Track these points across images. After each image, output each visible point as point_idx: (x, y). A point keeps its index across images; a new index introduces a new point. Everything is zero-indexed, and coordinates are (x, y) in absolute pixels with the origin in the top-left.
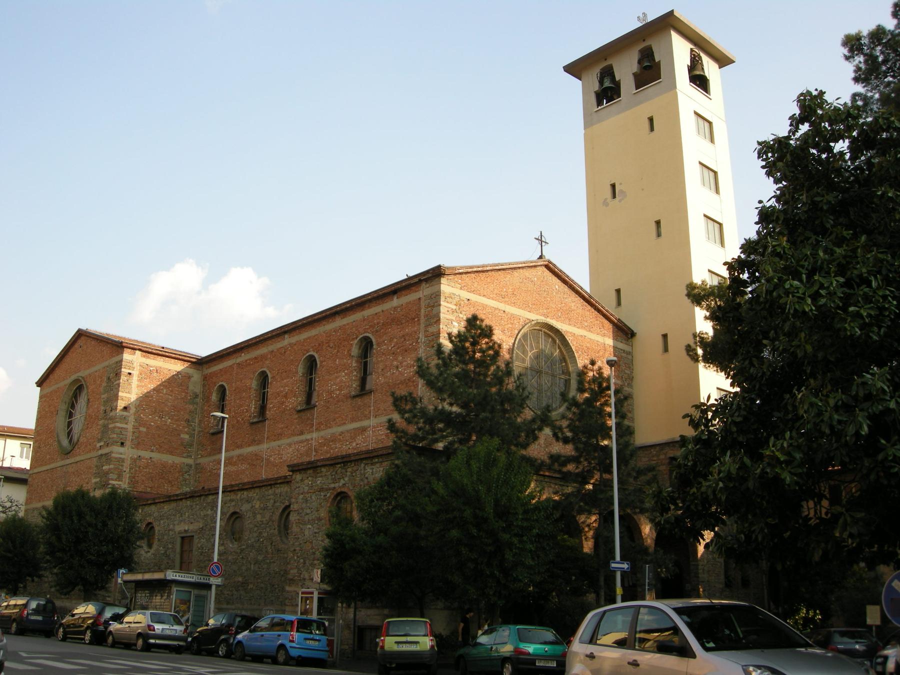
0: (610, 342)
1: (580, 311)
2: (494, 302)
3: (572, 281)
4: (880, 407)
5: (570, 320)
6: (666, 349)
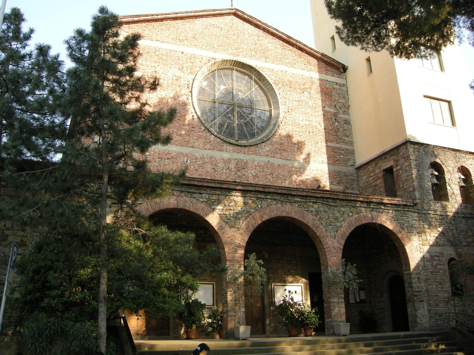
1: (280, 50)
3: (266, 24)
4: (31, 121)
5: (266, 58)
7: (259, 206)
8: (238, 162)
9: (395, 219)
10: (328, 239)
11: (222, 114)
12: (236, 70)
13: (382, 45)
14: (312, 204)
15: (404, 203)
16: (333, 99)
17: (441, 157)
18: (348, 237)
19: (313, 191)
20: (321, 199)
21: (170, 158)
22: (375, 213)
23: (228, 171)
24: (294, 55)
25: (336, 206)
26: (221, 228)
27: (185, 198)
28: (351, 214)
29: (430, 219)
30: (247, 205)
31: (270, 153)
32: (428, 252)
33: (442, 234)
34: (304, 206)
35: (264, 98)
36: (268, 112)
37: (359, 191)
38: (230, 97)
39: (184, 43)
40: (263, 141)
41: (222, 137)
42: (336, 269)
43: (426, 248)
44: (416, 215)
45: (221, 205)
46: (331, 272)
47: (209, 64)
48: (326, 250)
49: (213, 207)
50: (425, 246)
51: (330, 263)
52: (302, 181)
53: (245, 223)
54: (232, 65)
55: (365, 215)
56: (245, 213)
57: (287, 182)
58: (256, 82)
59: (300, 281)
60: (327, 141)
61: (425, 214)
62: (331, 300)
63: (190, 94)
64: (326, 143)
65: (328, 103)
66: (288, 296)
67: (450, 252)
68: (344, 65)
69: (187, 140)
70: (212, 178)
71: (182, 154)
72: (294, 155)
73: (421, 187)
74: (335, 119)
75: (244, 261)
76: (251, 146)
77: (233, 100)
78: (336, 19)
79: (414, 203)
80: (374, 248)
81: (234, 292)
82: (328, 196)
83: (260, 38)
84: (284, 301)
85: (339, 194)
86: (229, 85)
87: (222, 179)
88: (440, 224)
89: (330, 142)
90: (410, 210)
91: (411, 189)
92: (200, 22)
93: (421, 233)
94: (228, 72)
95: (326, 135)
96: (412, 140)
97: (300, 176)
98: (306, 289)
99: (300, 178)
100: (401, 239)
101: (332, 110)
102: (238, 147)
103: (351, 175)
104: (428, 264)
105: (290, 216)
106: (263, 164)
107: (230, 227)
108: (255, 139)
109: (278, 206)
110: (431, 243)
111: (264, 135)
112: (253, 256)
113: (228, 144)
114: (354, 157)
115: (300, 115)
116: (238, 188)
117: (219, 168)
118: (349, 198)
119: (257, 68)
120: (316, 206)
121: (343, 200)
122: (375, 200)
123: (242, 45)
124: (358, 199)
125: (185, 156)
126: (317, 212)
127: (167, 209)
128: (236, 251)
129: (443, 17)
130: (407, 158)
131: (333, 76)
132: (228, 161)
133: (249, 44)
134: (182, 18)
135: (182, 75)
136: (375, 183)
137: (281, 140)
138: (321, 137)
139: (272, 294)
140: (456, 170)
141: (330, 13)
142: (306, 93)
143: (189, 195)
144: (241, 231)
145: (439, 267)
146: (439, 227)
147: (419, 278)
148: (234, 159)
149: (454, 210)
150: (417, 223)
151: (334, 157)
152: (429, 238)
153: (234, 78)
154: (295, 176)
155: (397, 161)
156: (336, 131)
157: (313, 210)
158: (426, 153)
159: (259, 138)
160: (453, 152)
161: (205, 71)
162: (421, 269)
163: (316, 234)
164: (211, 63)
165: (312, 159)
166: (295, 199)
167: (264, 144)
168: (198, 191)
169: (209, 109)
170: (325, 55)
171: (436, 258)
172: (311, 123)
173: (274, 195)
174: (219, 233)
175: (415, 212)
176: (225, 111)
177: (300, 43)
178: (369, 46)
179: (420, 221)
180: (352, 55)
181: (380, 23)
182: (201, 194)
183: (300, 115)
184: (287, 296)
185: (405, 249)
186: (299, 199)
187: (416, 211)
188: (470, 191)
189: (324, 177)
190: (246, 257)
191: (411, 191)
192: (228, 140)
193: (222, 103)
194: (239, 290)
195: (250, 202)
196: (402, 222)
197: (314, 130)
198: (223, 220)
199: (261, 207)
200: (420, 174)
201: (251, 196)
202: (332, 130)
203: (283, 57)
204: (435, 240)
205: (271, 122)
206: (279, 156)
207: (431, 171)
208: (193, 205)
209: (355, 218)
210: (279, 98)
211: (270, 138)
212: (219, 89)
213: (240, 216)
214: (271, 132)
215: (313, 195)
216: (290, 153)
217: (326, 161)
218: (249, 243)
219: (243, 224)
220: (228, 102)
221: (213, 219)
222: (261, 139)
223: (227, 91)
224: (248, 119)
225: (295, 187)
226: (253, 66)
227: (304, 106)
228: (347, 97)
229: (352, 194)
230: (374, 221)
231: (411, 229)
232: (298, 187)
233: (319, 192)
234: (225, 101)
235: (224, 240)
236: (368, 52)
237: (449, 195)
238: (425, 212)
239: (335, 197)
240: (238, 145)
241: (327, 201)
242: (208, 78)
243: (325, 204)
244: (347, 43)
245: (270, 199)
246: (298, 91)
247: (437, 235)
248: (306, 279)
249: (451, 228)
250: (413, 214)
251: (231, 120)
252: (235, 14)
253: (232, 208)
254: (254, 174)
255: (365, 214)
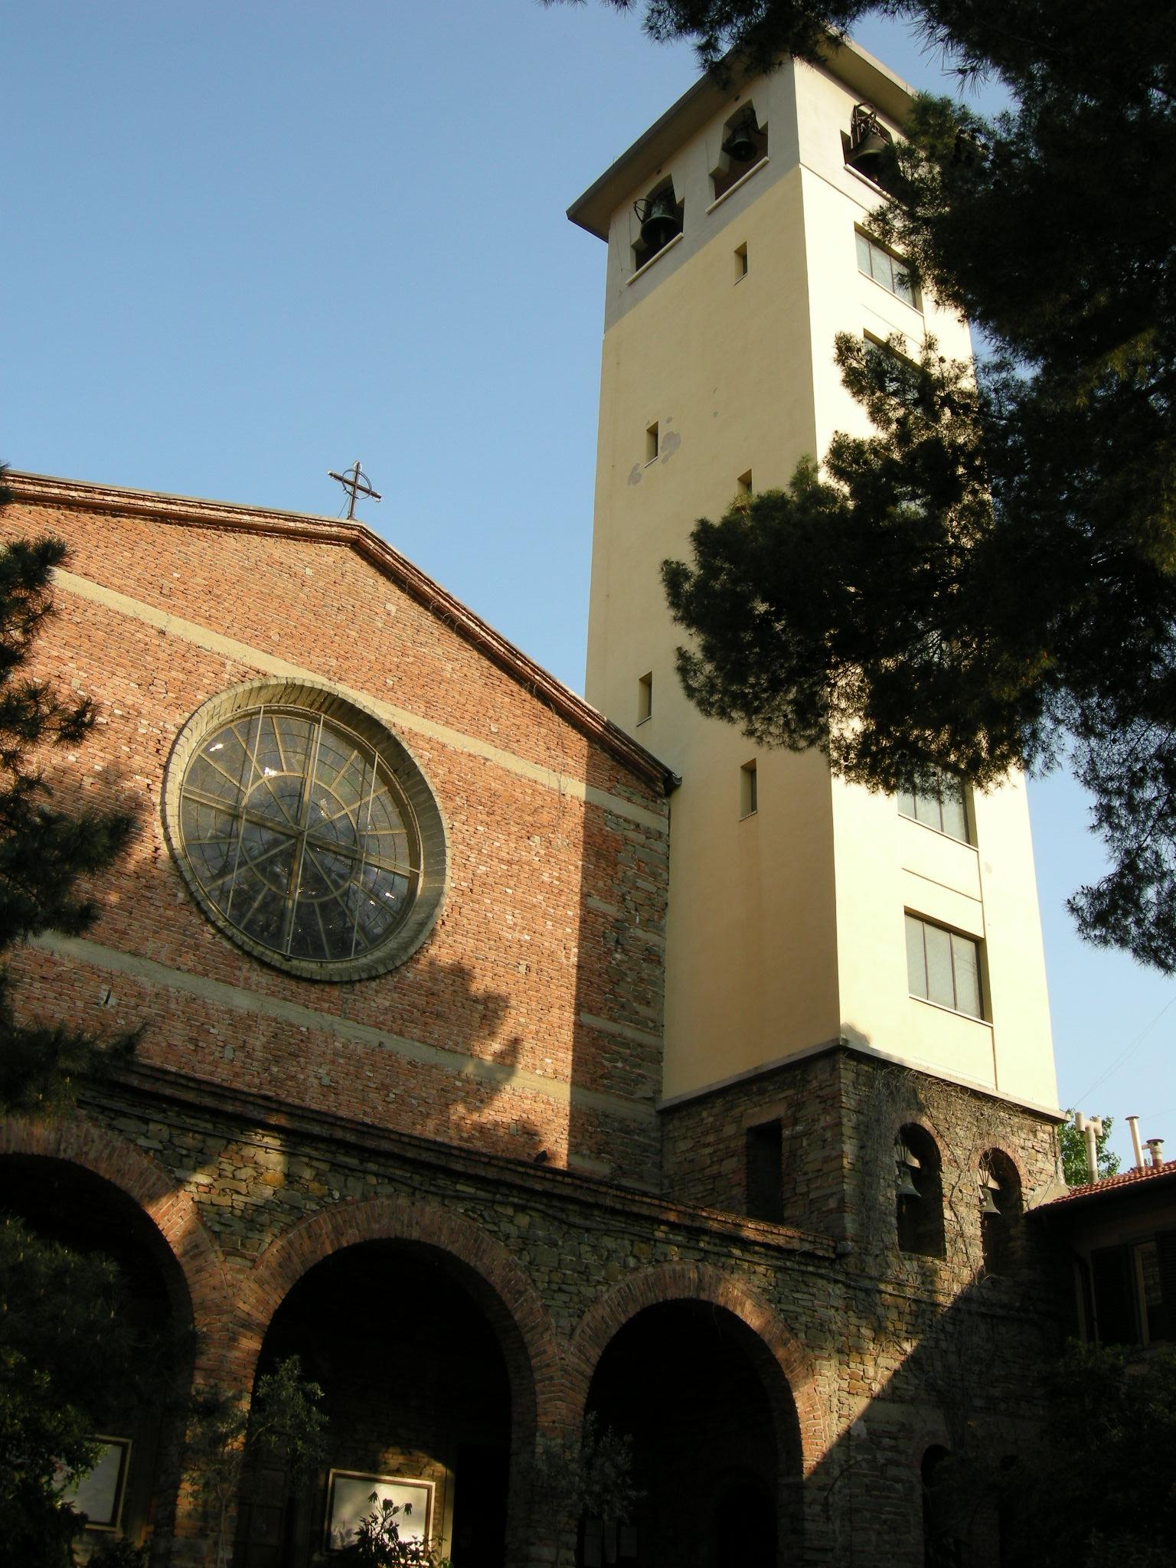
0: (576, 789)
1: (477, 688)
2: (125, 599)
3: (447, 597)
5: (429, 704)
6: (752, 804)
7: (337, 1195)
8: (280, 1030)
9: (771, 1298)
10: (547, 1337)
11: (253, 858)
12: (326, 725)
13: (812, 732)
14: (510, 1211)
15: (807, 1247)
16: (620, 875)
17: (935, 1113)
18: (614, 1338)
19: (521, 1169)
20: (545, 1201)
21: (52, 976)
22: (710, 1269)
23: (241, 1055)
24: (518, 712)
25: (588, 1230)
26: (195, 1249)
27: (87, 1125)
28: (632, 1262)
29: (880, 1310)
30: (296, 1186)
31: (389, 1017)
32: (866, 1417)
33: (912, 1363)
34: (486, 1214)
35: (402, 831)
36: (405, 882)
37: (660, 1185)
38: (287, 812)
39: (174, 601)
40: (374, 973)
41: (241, 938)
42: (563, 1446)
43: (860, 1404)
44: (839, 1290)
45: (208, 1169)
46: (547, 1451)
47: (240, 689)
48: (537, 1376)
49: (179, 1173)
50: (857, 1399)
51: (544, 1421)
52: (481, 1129)
53: (279, 1243)
54: (317, 705)
55: (680, 1271)
56: (286, 1210)
57: (431, 1125)
58: (381, 773)
59: (428, 1471)
60: (579, 1009)
61: (867, 1291)
62: (534, 1551)
63: (160, 772)
64: (577, 1013)
65: (601, 884)
66: (380, 1520)
67: (932, 1424)
68: (670, 773)
69: (121, 926)
70: (183, 1072)
71: (94, 970)
72: (467, 1038)
73: (866, 1202)
74: (617, 942)
75: (257, 1379)
76: (331, 983)
77: (297, 822)
78: (689, 626)
79: (839, 1250)
80: (697, 1387)
81: (206, 1485)
82: (567, 1191)
83: (422, 638)
84: (364, 1533)
85: (603, 1189)
86: (293, 770)
87: (217, 1081)
88: (910, 1328)
89: (590, 1012)
90: (823, 1271)
91: (832, 1204)
92: (239, 546)
93: (848, 1351)
94: (298, 725)
95: (578, 988)
96: (854, 1045)
97: (479, 1110)
98: (441, 1500)
99: (475, 1117)
100: (783, 1366)
101: (612, 910)
102: (287, 981)
103: (643, 1131)
104: (859, 1458)
105: (433, 1240)
106: (360, 1050)
107: (227, 1254)
108: (348, 965)
109: (399, 1202)
110: (876, 1388)
111: (378, 954)
112: (290, 1367)
113: (255, 966)
114: (659, 1071)
115: (508, 909)
116: (273, 1120)
117: (211, 1039)
118: (635, 1209)
119: (394, 732)
120: (523, 1220)
121: (613, 1211)
122: (715, 1226)
123: (360, 649)
124: (664, 1217)
125: (105, 980)
126: (526, 1241)
127: (17, 1155)
128: (234, 1339)
129: (1026, 682)
130: (832, 1101)
131: (629, 800)
132: (244, 1023)
133: (384, 649)
134: (183, 520)
135: (146, 705)
136: (715, 1169)
137: (434, 980)
138: (564, 991)
139: (324, 1506)
140: (976, 1159)
141: (674, 605)
142: (537, 839)
143: (103, 1120)
144: (262, 1271)
145: (892, 1471)
146: (907, 1339)
147: (826, 1505)
148: (268, 1019)
149: (956, 1288)
150: (838, 1318)
151: (596, 1062)
152: (871, 1372)
153: (316, 750)
154: (461, 1109)
155: (797, 1106)
156: (616, 978)
157: (513, 1231)
158: (891, 1093)
159: (363, 961)
160: (974, 1102)
161: (224, 706)
162: (836, 1472)
163: (509, 1315)
164: (248, 686)
165: (524, 1060)
166: (459, 1187)
167: (374, 984)
168: (137, 1111)
169: (211, 838)
170: (618, 731)
171: (886, 1441)
172: (538, 938)
173: (391, 1163)
174: (185, 1268)
175: (836, 1281)
176: (266, 851)
177: (545, 676)
178: (772, 729)
179: (851, 1313)
180: (705, 748)
181: (813, 669)
182: (147, 1121)
183: (508, 909)
184: (376, 1519)
185: (792, 1402)
186: (472, 1190)
187: (840, 1277)
188: (1012, 1232)
189: (553, 1126)
190: (265, 1363)
191: (831, 1211)
192: (258, 950)
193: (259, 824)
194: (224, 1480)
195: (308, 1174)
196: (792, 1308)
197: (545, 965)
198: (204, 1224)
199: (343, 1198)
200: (867, 1158)
201: (314, 1153)
202: (600, 975)
203: (482, 711)
204: (890, 1381)
205: (412, 916)
206: (417, 1032)
207: (899, 1153)
208: (110, 1156)
209: (646, 1276)
210: (448, 843)
211: (397, 968)
212: (258, 777)
213: (265, 1218)
214: (404, 947)
215: (518, 1181)
216: (455, 1030)
217: (568, 1071)
218: (282, 1315)
219: (271, 1247)
220: (279, 823)
221: (172, 1216)
222: (369, 968)
223: (281, 790)
224: (336, 894)
225: (455, 1143)
226: (383, 723)
227: (524, 881)
228: (665, 875)
229: (645, 1194)
230: (704, 1296)
231: (817, 1338)
232: (465, 1145)
233: (539, 1173)
234: (272, 820)
235: (196, 1297)
236: (765, 748)
237: (948, 1236)
238: (868, 1284)
239: (590, 1200)
240: (288, 974)
241: (563, 1210)
242: (230, 731)
243: (555, 1218)
244: (705, 707)
245: (376, 1175)
246: (514, 829)
247: (896, 1365)
248: (446, 1464)
249: (943, 1345)
250: (830, 1288)
251: (280, 886)
252: (356, 546)
253: (242, 1187)
254: (326, 1081)
255: (678, 1268)
